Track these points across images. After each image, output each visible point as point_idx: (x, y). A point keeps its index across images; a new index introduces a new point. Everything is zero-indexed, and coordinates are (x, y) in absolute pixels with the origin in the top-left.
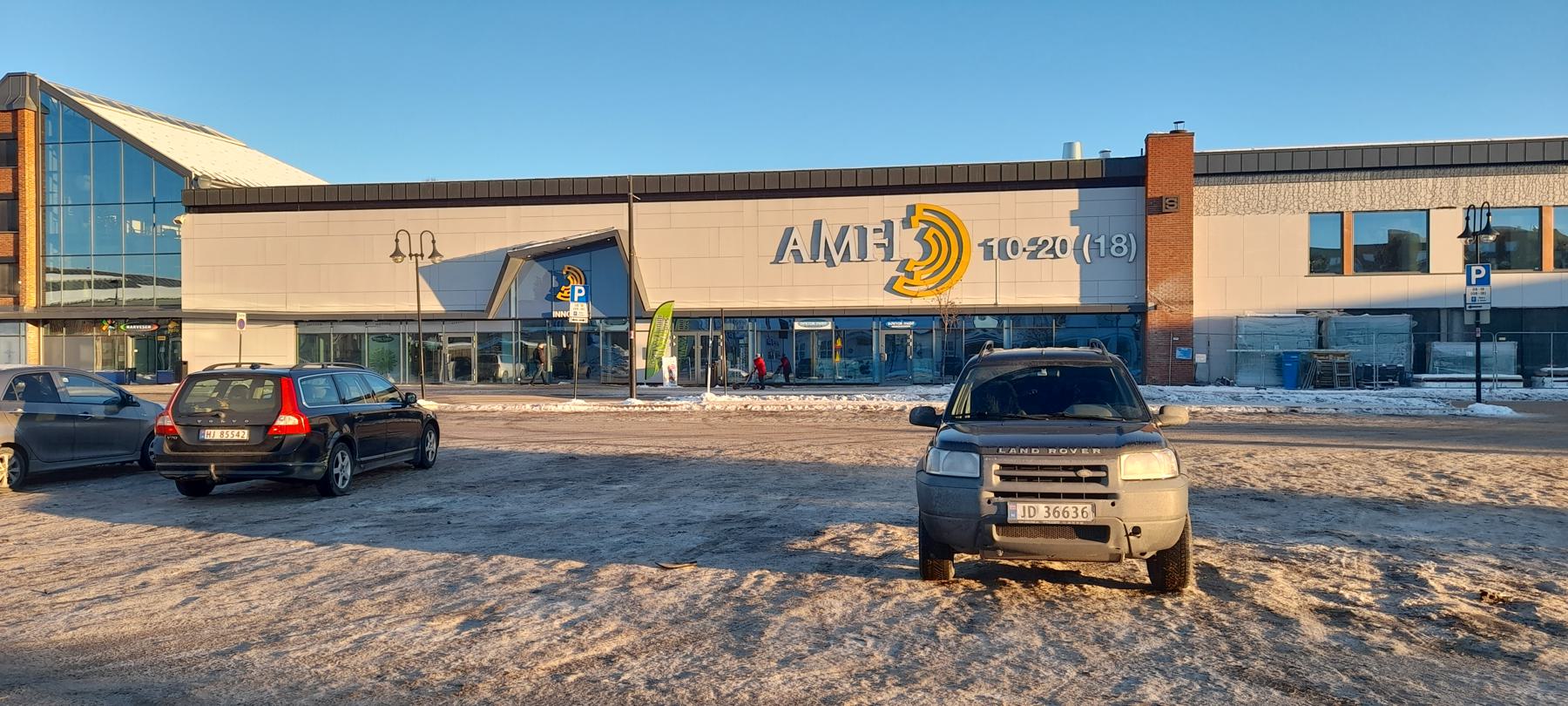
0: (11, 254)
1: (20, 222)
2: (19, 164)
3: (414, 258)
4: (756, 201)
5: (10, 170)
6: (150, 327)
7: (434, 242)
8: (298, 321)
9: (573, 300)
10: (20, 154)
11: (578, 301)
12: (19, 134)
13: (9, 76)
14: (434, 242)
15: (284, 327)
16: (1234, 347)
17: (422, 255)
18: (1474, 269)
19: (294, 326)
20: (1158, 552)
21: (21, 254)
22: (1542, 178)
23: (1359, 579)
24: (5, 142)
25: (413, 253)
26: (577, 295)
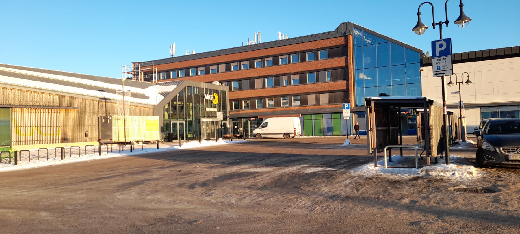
0: (345, 88)
1: (349, 76)
2: (348, 55)
3: (458, 84)
4: (496, 60)
5: (344, 58)
6: (405, 112)
7: (468, 76)
8: (481, 106)
9: (344, 109)
10: (348, 51)
11: (346, 109)
12: (348, 44)
13: (342, 24)
14: (468, 76)
15: (474, 109)
16: (255, 121)
17: (462, 82)
18: (345, 105)
19: (479, 109)
20: (172, 141)
21: (350, 88)
22: (340, 89)
23: (340, 164)
24: (341, 48)
25: (458, 82)
26: (345, 107)
